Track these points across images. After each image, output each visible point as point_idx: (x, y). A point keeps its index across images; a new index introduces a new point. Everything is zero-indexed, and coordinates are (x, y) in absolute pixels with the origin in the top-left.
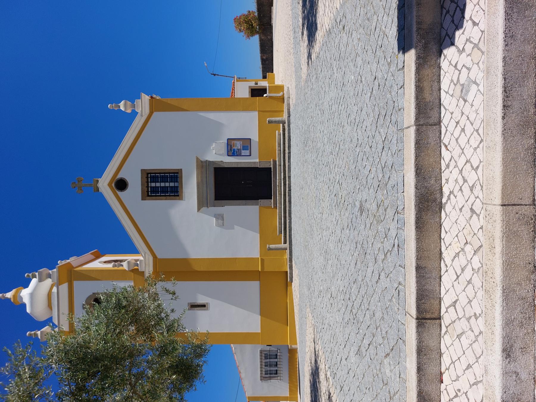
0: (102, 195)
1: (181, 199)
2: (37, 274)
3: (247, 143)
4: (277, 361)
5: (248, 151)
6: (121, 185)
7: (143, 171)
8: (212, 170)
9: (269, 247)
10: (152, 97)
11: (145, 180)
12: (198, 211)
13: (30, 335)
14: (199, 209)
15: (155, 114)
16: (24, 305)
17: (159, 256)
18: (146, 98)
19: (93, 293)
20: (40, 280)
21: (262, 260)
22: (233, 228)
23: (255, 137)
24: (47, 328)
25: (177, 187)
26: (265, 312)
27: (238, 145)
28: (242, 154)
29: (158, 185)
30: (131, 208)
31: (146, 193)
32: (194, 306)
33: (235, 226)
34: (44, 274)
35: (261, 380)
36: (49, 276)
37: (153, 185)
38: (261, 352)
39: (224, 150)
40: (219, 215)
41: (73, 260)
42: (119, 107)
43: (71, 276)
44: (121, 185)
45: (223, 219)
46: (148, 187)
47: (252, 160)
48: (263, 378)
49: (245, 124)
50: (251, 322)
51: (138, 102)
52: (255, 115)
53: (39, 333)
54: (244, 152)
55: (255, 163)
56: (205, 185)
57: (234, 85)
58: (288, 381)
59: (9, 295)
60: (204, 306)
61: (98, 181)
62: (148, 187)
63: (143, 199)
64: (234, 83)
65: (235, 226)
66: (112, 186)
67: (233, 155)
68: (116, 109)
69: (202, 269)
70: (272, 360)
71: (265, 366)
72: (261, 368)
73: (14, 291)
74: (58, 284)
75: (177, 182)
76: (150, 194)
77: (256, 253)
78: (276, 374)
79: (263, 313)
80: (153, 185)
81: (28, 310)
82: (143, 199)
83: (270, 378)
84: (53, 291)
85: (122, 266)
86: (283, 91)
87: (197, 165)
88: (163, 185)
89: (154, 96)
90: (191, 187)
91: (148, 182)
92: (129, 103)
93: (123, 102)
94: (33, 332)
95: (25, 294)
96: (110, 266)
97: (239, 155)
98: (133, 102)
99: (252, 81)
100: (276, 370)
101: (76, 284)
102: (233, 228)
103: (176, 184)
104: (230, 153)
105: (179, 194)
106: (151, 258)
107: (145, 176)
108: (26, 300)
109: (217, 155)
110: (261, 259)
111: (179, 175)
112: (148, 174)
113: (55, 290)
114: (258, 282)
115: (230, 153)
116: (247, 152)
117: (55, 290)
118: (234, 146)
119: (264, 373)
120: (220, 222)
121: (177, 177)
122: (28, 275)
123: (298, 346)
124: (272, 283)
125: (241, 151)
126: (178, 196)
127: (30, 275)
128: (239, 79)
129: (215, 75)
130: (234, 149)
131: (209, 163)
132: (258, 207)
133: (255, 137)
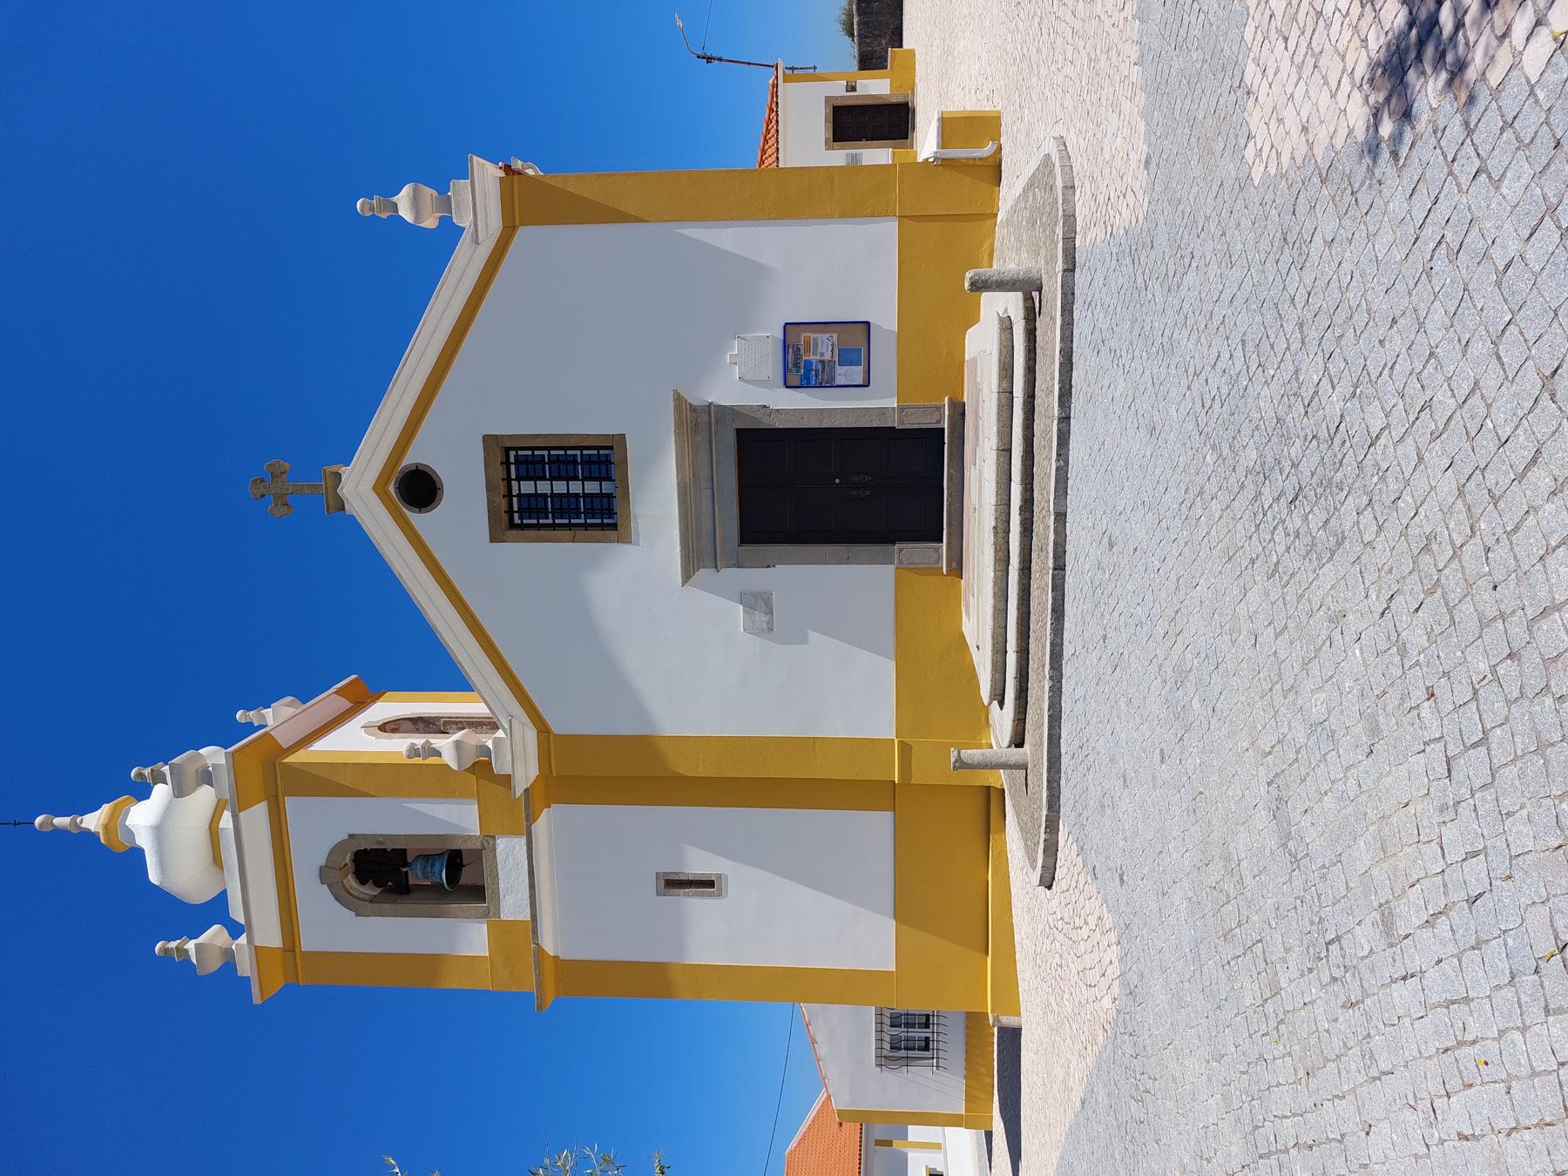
0: (353, 524)
1: (626, 539)
2: (166, 769)
3: (855, 337)
4: (956, 1036)
5: (860, 369)
6: (418, 489)
7: (489, 440)
8: (731, 439)
9: (959, 759)
10: (508, 169)
11: (500, 472)
12: (684, 582)
13: (166, 951)
14: (687, 577)
15: (524, 234)
16: (138, 853)
17: (557, 727)
18: (487, 173)
19: (351, 836)
20: (180, 791)
21: (906, 749)
22: (805, 641)
23: (885, 315)
24: (214, 935)
25: (610, 496)
27: (824, 347)
28: (839, 381)
29: (544, 487)
30: (452, 561)
31: (505, 517)
32: (674, 884)
34: (190, 770)
36: (206, 777)
37: (527, 487)
40: (755, 595)
41: (278, 717)
42: (395, 206)
43: (275, 780)
44: (418, 489)
46: (509, 496)
47: (875, 400)
48: (884, 1061)
49: (846, 269)
50: (868, 940)
51: (460, 189)
53: (191, 945)
54: (843, 374)
55: (883, 411)
56: (706, 493)
57: (775, 94)
58: (962, 1072)
59: (92, 822)
60: (711, 884)
61: (338, 476)
62: (509, 496)
63: (494, 538)
64: (775, 86)
66: (388, 494)
67: (805, 384)
68: (384, 216)
69: (701, 773)
72: (880, 1031)
73: (106, 808)
74: (239, 802)
75: (609, 479)
76: (517, 520)
77: (881, 723)
78: (926, 1048)
79: (898, 915)
80: (527, 487)
81: (154, 877)
82: (494, 538)
83: (908, 1061)
84: (222, 825)
85: (438, 754)
86: (996, 137)
88: (560, 489)
89: (518, 164)
90: (657, 494)
91: (508, 480)
92: (428, 193)
93: (406, 191)
94: (173, 944)
95: (141, 818)
96: (398, 746)
97: (829, 383)
98: (443, 190)
99: (838, 77)
102: (805, 641)
103: (607, 487)
104: (796, 380)
105: (619, 520)
106: (531, 735)
107: (500, 458)
108: (144, 840)
109: (747, 383)
110: (901, 743)
111: (615, 458)
112: (507, 450)
113: (226, 821)
114: (889, 814)
117: (226, 821)
118: (808, 350)
119: (887, 1046)
120: (761, 618)
121: (607, 462)
122: (140, 775)
124: (944, 829)
125: (833, 370)
126: (614, 527)
127: (147, 771)
128: (795, 73)
129: (709, 59)
130: (809, 363)
132: (891, 568)
133: (885, 315)
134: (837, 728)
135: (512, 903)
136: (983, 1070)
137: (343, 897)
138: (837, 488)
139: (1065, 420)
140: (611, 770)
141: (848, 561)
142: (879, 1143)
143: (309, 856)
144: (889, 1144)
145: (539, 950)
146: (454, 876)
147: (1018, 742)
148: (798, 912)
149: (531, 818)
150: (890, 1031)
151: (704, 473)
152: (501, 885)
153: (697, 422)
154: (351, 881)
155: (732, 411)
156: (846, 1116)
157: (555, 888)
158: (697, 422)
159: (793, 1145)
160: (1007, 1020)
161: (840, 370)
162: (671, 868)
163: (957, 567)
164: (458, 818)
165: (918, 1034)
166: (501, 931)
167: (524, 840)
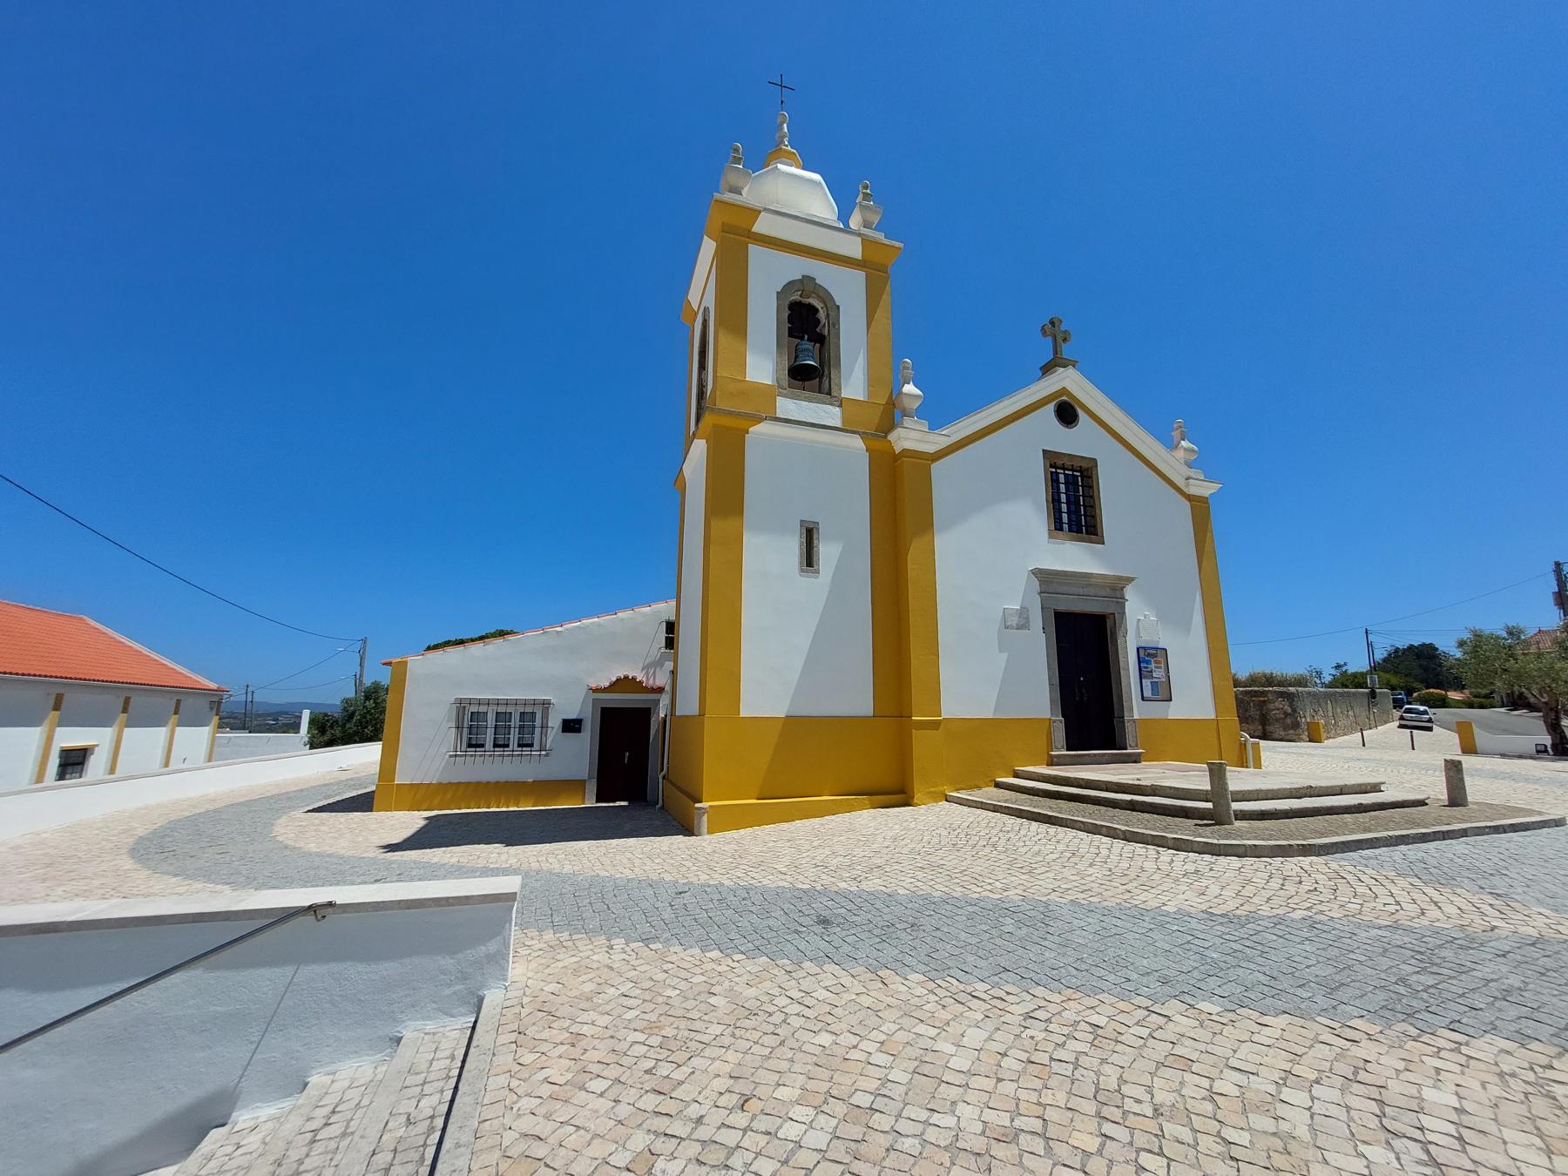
1: (1051, 536)
3: (1163, 693)
17: (936, 468)
21: (935, 725)
32: (810, 535)
33: (1005, 656)
38: (546, 705)
39: (1148, 639)
44: (1067, 413)
45: (1019, 627)
47: (1137, 709)
48: (461, 705)
52: (1209, 713)
55: (1131, 709)
65: (1005, 656)
70: (490, 733)
71: (522, 714)
72: (516, 703)
74: (866, 242)
79: (792, 722)
87: (1120, 578)
88: (1074, 501)
90: (1074, 557)
100: (531, 745)
106: (931, 449)
109: (1140, 622)
116: (1147, 693)
120: (1014, 621)
123: (705, 842)
124: (880, 753)
126: (1058, 526)
131: (1120, 602)
134: (948, 672)
135: (788, 406)
140: (900, 505)
142: (127, 701)
143: (826, 275)
144: (125, 710)
146: (809, 372)
149: (864, 436)
150: (516, 712)
151: (1092, 591)
153: (1115, 588)
154: (796, 297)
157: (805, 449)
158: (1115, 588)
159: (93, 623)
163: (1052, 762)
164: (853, 382)
165: (514, 737)
166: (766, 395)
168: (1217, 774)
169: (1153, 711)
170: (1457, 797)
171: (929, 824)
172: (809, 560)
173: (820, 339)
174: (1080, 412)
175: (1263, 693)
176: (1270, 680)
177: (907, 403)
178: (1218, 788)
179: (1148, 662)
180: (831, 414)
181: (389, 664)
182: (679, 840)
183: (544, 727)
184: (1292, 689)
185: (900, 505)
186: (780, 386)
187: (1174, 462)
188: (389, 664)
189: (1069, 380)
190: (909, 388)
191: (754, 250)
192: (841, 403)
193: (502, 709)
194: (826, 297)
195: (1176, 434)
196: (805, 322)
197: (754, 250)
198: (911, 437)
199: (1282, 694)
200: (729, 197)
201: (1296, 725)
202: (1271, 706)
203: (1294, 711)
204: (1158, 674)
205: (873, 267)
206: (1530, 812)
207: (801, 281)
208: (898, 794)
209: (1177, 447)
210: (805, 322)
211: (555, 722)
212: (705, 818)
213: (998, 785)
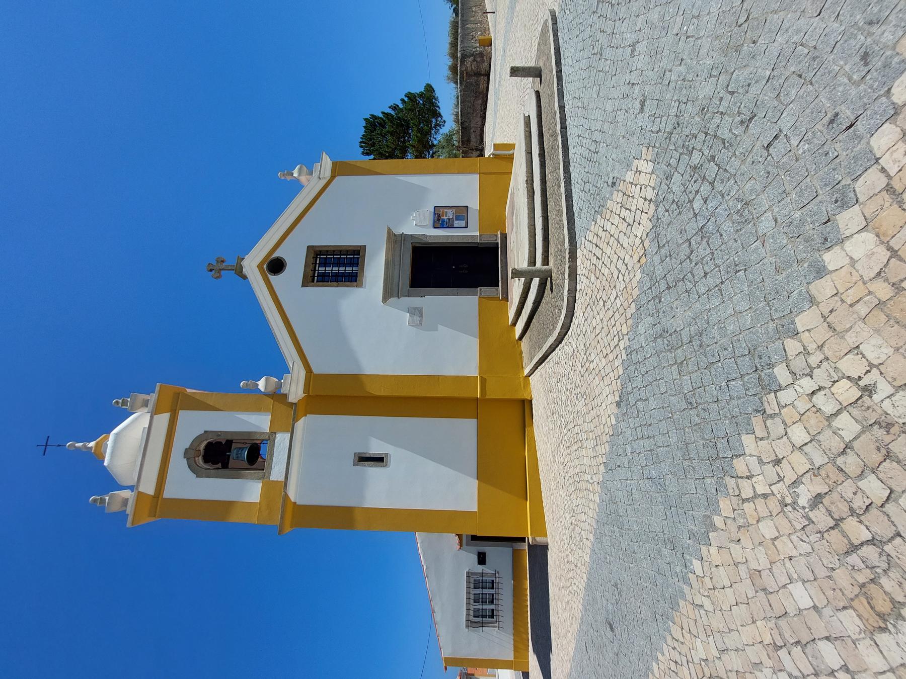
1: (360, 286)
3: (462, 212)
4: (509, 572)
14: (385, 299)
17: (316, 370)
19: (206, 432)
21: (483, 381)
23: (474, 204)
26: (484, 474)
32: (365, 459)
33: (440, 327)
35: (468, 626)
36: (145, 404)
37: (322, 269)
38: (469, 575)
39: (429, 220)
40: (415, 309)
44: (276, 266)
45: (421, 316)
48: (470, 624)
56: (397, 267)
62: (315, 270)
65: (440, 327)
67: (442, 227)
72: (468, 604)
74: (155, 412)
77: (472, 370)
78: (492, 602)
81: (106, 464)
88: (336, 266)
90: (375, 270)
100: (493, 610)
101: (183, 415)
106: (303, 373)
109: (418, 226)
115: (437, 225)
116: (463, 223)
120: (417, 319)
122: (117, 403)
123: (550, 541)
124: (500, 421)
132: (477, 298)
133: (474, 204)
134: (450, 371)
135: (277, 473)
136: (522, 629)
137: (193, 467)
138: (452, 266)
139: (559, 72)
140: (340, 395)
141: (457, 294)
143: (183, 441)
145: (286, 496)
147: (546, 261)
148: (427, 474)
149: (295, 420)
151: (397, 259)
152: (274, 460)
153: (395, 240)
154: (200, 460)
155: (412, 236)
156: (452, 662)
157: (306, 462)
158: (395, 240)
160: (540, 540)
161: (456, 222)
162: (361, 450)
164: (258, 422)
167: (289, 435)
168: (517, 274)
169: (474, 218)
170: (535, 73)
171: (544, 390)
172: (379, 460)
173: (229, 443)
174: (275, 255)
175: (462, 73)
176: (454, 69)
177: (271, 389)
178: (528, 276)
179: (443, 221)
180: (282, 439)
181: (446, 668)
182: (550, 554)
183: (482, 574)
184: (459, 55)
185: (340, 395)
186: (263, 478)
187: (311, 185)
188: (446, 668)
189: (252, 263)
190: (261, 384)
191: (168, 494)
192: (273, 433)
193: (472, 586)
194: (198, 439)
195: (289, 178)
196: (218, 454)
197: (168, 494)
198: (295, 389)
199: (462, 62)
200: (129, 510)
201: (481, 55)
202: (469, 69)
203: (472, 55)
204: (450, 214)
205: (176, 404)
206: (544, 32)
207: (188, 459)
208: (525, 406)
209: (297, 181)
210: (218, 454)
211: (480, 569)
212: (538, 539)
213: (521, 338)
